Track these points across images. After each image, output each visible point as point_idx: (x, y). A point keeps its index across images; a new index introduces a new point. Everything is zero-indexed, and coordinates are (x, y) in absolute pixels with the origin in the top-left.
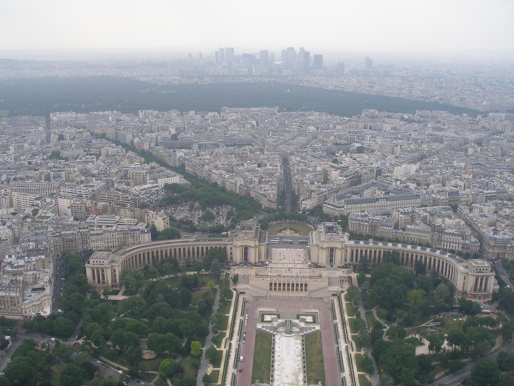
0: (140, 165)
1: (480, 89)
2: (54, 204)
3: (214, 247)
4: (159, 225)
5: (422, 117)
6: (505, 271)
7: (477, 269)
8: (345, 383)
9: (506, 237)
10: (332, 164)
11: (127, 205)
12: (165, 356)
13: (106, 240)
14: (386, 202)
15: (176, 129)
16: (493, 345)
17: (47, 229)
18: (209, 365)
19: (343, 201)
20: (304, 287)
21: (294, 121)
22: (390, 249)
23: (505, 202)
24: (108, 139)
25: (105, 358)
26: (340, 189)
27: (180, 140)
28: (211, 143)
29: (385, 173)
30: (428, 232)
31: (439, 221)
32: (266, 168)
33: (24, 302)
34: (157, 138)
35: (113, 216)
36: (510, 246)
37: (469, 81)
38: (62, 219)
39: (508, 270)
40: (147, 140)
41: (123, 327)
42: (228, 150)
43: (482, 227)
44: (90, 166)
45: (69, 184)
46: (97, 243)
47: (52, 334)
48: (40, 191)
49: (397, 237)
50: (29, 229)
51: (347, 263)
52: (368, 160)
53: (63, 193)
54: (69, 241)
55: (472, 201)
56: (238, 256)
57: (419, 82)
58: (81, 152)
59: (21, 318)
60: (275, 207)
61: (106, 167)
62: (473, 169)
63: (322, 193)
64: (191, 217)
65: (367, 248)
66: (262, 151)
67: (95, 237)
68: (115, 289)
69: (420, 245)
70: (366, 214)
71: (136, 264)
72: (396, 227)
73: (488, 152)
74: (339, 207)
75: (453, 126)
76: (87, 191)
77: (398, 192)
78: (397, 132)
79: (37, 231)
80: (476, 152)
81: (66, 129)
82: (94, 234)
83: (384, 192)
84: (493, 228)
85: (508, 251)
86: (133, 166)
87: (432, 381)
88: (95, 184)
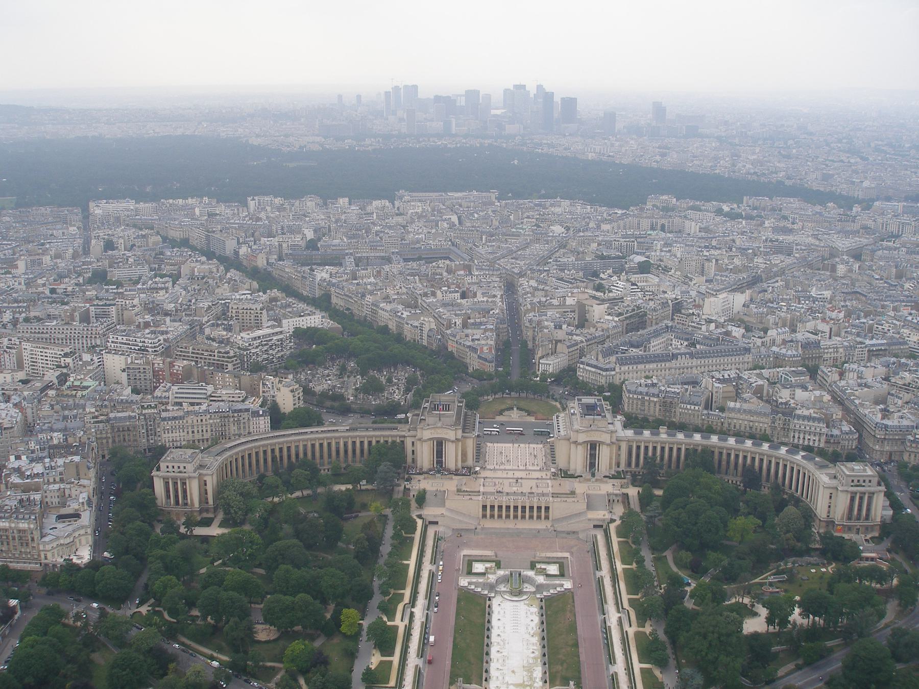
0: (251, 294)
1: (858, 160)
2: (97, 364)
3: (382, 441)
4: (284, 402)
5: (755, 208)
6: (903, 485)
7: (853, 481)
8: (618, 683)
9: (905, 423)
10: (594, 292)
11: (227, 365)
12: (295, 636)
13: (190, 428)
14: (690, 361)
15: (315, 231)
16: (881, 615)
17: (84, 410)
18: (374, 651)
19: (613, 359)
20: (543, 512)
21: (525, 215)
22: (698, 445)
23: (903, 360)
24: (193, 248)
25: (188, 638)
26: (608, 337)
27: (322, 251)
28: (378, 254)
29: (687, 309)
30: (765, 414)
31: (784, 395)
32: (475, 300)
33: (43, 540)
34: (280, 246)
35: (202, 385)
36: (912, 439)
37: (839, 145)
38: (110, 391)
39: (908, 482)
40: (262, 250)
41: (220, 583)
42: (408, 267)
43: (861, 405)
44: (161, 296)
45: (123, 328)
46: (174, 435)
47: (94, 597)
48: (72, 341)
49: (710, 423)
50: (53, 409)
51: (620, 469)
52: (659, 286)
53: (113, 345)
54: (123, 431)
55: (843, 359)
56: (425, 456)
57: (749, 146)
58: (145, 271)
59: (37, 567)
60: (492, 370)
61: (190, 298)
62: (845, 301)
63: (576, 344)
64: (342, 387)
65: (657, 442)
66: (468, 269)
67: (170, 422)
68: (205, 515)
69: (752, 437)
70: (655, 381)
71: (243, 471)
72: (708, 405)
73: (873, 271)
74: (607, 370)
75: (810, 225)
76: (156, 340)
77: (712, 342)
78: (709, 236)
79: (66, 413)
80: (851, 271)
81: (119, 230)
82: (169, 417)
83: (686, 343)
84: (882, 406)
85: (908, 449)
86: (238, 297)
87: (773, 681)
88: (169, 329)
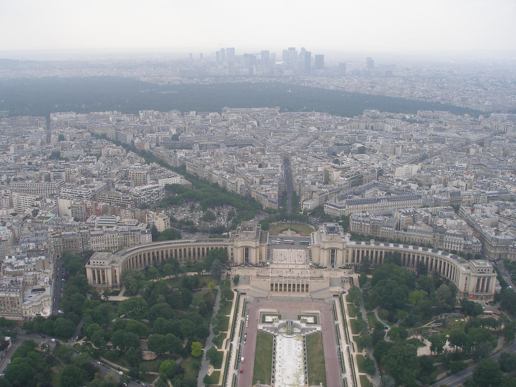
0: (141, 165)
1: (482, 90)
2: (54, 205)
3: (214, 248)
4: (160, 226)
5: (424, 117)
6: (507, 272)
7: (479, 270)
8: (347, 384)
9: (508, 237)
10: (333, 164)
11: (127, 205)
12: (165, 357)
13: (107, 240)
14: (387, 203)
15: (177, 130)
16: (495, 346)
17: (47, 230)
18: (210, 366)
19: (344, 201)
20: (305, 287)
21: (295, 121)
22: (392, 250)
23: (507, 202)
24: (109, 140)
25: (106, 359)
26: (341, 189)
27: (181, 141)
28: (212, 143)
29: (386, 173)
30: (429, 233)
31: (440, 222)
32: (267, 168)
33: (24, 303)
34: (157, 138)
35: (113, 217)
36: (512, 246)
37: (471, 82)
38: (62, 220)
39: (510, 271)
40: (147, 140)
41: (124, 328)
42: (229, 150)
43: (484, 227)
44: (90, 166)
45: (69, 184)
46: (98, 244)
47: (53, 335)
48: (41, 192)
49: (399, 237)
50: (30, 230)
51: (348, 264)
52: (370, 160)
53: (63, 194)
54: (69, 242)
55: (473, 202)
56: (239, 256)
57: (421, 82)
58: (81, 152)
59: (21, 318)
60: (276, 208)
61: (107, 167)
62: (474, 169)
63: (324, 193)
64: (192, 218)
65: (369, 249)
66: (263, 151)
67: (95, 237)
68: (115, 289)
69: (422, 245)
70: (368, 214)
71: (137, 265)
72: (398, 228)
73: (490, 152)
74: (341, 208)
75: (455, 126)
76: (88, 191)
77: (400, 192)
78: (398, 132)
79: (37, 232)
80: (478, 152)
81: (67, 129)
82: (95, 234)
83: (385, 193)
84: (495, 228)
85: (510, 252)
86: (134, 167)
87: (434, 382)
88: (95, 185)
